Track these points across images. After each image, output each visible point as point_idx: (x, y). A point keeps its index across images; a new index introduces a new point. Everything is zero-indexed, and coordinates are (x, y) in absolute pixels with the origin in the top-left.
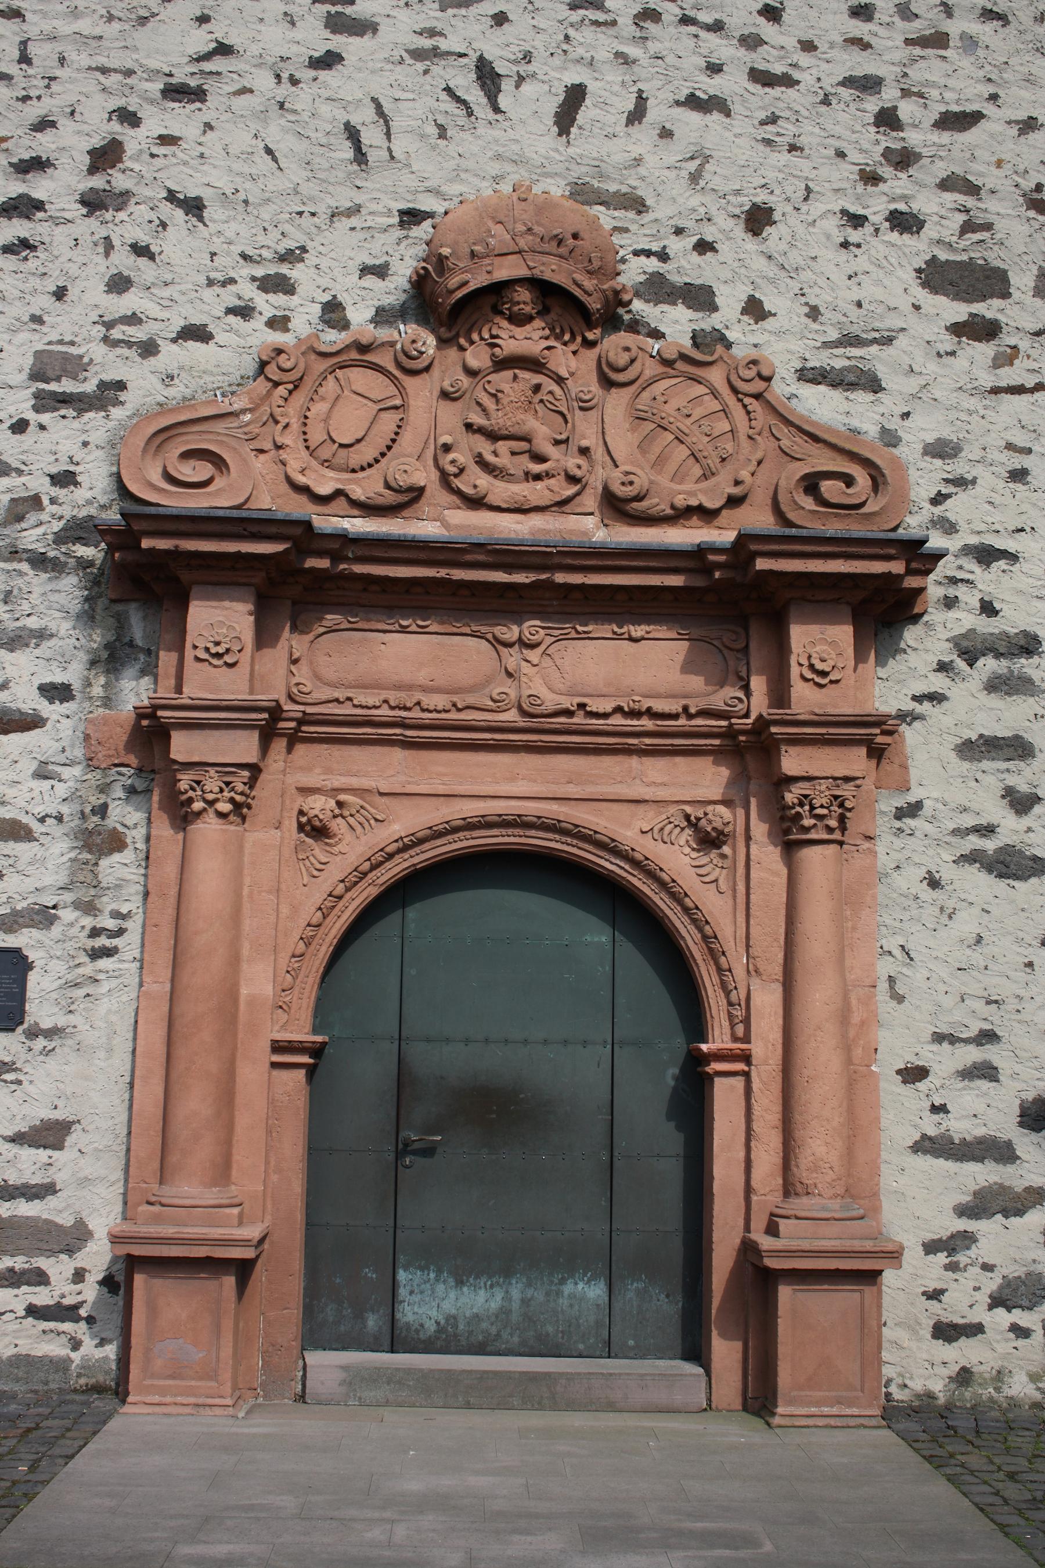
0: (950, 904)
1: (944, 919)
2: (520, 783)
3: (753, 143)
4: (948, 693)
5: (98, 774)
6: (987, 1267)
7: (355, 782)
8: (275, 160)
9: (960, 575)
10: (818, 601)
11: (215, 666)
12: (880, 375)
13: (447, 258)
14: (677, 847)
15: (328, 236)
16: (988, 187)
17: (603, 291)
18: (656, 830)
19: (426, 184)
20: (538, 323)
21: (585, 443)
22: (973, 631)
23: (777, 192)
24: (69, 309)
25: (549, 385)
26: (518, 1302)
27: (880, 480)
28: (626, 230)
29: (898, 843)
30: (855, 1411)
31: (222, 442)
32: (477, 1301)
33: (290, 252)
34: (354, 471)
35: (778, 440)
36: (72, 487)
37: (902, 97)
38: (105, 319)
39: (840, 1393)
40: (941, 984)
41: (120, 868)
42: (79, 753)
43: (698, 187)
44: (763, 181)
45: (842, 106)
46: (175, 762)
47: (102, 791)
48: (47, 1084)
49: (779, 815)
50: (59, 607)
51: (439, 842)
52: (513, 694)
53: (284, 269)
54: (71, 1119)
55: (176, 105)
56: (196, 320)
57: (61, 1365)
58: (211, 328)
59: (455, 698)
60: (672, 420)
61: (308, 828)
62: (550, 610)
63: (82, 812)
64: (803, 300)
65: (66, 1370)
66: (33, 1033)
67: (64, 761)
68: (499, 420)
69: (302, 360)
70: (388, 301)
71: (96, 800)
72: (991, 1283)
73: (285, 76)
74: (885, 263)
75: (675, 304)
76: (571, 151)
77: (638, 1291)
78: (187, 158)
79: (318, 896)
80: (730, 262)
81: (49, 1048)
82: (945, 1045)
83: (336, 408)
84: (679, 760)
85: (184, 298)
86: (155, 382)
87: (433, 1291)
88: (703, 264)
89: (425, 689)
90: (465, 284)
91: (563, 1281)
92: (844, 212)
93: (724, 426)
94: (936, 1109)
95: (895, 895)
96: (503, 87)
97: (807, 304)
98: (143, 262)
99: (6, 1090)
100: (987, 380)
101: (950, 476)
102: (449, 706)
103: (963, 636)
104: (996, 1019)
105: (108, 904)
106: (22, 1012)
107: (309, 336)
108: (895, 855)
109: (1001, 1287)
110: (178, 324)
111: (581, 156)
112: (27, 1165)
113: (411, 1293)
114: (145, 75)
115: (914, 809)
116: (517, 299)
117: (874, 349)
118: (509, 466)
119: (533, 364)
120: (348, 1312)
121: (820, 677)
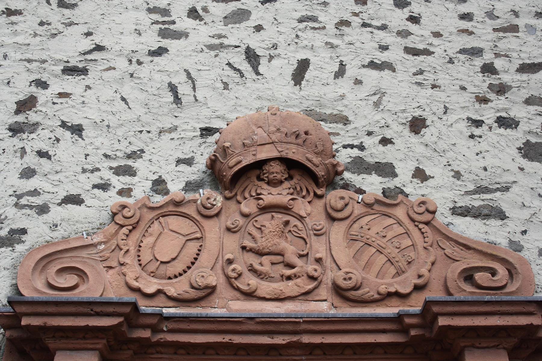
8: (127, 103)
12: (504, 209)
13: (228, 147)
19: (217, 114)
20: (286, 184)
21: (318, 255)
25: (294, 221)
27: (513, 272)
28: (338, 134)
33: (135, 152)
34: (170, 278)
35: (444, 249)
43: (379, 109)
44: (418, 105)
53: (130, 162)
58: (83, 197)
60: (374, 239)
64: (450, 168)
68: (262, 243)
70: (193, 178)
76: (302, 93)
78: (74, 104)
80: (403, 149)
83: (159, 240)
85: (68, 180)
88: (386, 151)
90: (240, 162)
92: (469, 119)
93: (407, 242)
98: (44, 160)
107: (143, 198)
110: (62, 194)
117: (498, 194)
119: (284, 209)
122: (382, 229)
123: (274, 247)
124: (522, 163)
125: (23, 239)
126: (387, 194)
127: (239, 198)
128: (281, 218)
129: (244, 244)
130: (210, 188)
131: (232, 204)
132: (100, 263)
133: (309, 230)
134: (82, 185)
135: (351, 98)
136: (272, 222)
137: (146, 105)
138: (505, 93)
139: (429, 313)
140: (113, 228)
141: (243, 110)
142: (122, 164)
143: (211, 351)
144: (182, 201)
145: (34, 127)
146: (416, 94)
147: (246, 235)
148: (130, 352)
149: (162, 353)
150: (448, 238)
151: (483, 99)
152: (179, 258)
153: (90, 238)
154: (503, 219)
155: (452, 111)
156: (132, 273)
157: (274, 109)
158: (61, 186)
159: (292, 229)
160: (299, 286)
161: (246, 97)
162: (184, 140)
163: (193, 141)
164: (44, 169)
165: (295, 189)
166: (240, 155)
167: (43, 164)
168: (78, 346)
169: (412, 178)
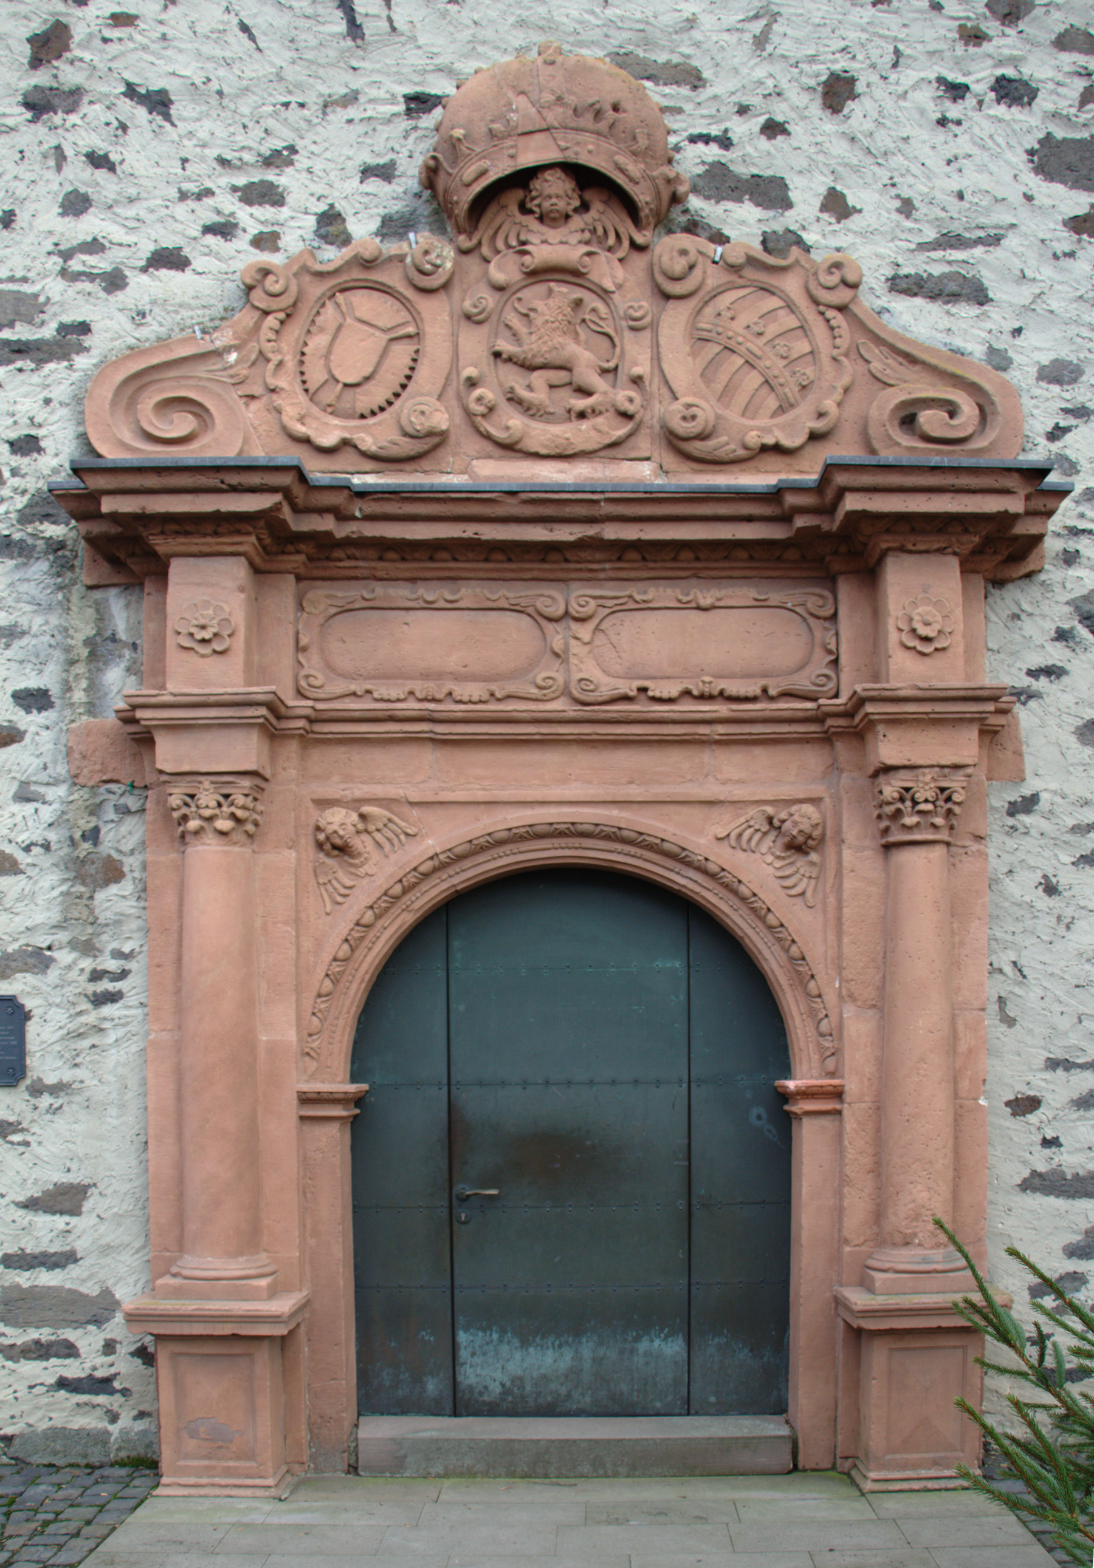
0: (1069, 912)
1: (1061, 930)
4: (1068, 667)
7: (379, 791)
8: (252, 38)
9: (1082, 525)
11: (203, 656)
12: (986, 283)
13: (459, 140)
14: (758, 855)
17: (653, 179)
18: (733, 836)
19: (438, 61)
20: (577, 222)
21: (637, 370)
23: (859, 57)
24: (18, 238)
25: (592, 301)
27: (988, 410)
28: (679, 111)
29: (1011, 843)
31: (204, 388)
32: (544, 1361)
33: (277, 153)
34: (363, 417)
35: (868, 362)
36: (35, 455)
38: (62, 248)
39: (937, 1455)
40: (1056, 1004)
41: (116, 900)
42: (62, 769)
43: (765, 54)
44: (842, 44)
46: (161, 772)
48: (57, 1145)
49: (876, 813)
50: (29, 599)
52: (560, 679)
53: (270, 176)
54: (86, 1182)
56: (169, 243)
57: (101, 1438)
58: (186, 252)
59: (493, 687)
60: (740, 339)
61: (328, 846)
62: (602, 575)
63: (72, 839)
64: (893, 192)
65: (105, 1443)
66: (37, 1090)
67: (46, 779)
68: (533, 346)
70: (396, 208)
71: (86, 823)
74: (990, 143)
75: (740, 200)
76: (610, 12)
78: (145, 41)
79: (343, 926)
80: (805, 147)
81: (56, 1105)
82: (1060, 1072)
83: (338, 341)
85: (153, 217)
86: (123, 322)
88: (773, 151)
89: (458, 678)
90: (483, 173)
91: (637, 1339)
92: (941, 80)
93: (802, 346)
94: (1047, 1143)
95: (1007, 904)
98: (101, 174)
99: (13, 1153)
101: (1069, 406)
102: (485, 696)
103: (1085, 598)
105: (108, 942)
107: (301, 253)
108: (1006, 858)
110: (147, 249)
111: (622, 19)
112: (46, 1231)
113: (473, 1354)
115: (1029, 803)
116: (548, 191)
117: (978, 251)
118: (547, 402)
119: (571, 274)
120: (405, 1376)
121: (924, 644)
122: (756, 320)
123: (554, 353)
124: (1031, 185)
125: (86, 345)
126: (770, 245)
127: (485, 250)
128: (565, 293)
129: (497, 348)
130: (431, 231)
131: (472, 263)
132: (232, 389)
133: (621, 319)
134: (182, 226)
135: (708, 27)
136: (550, 303)
137: (292, 41)
138: (1018, 19)
139: (828, 488)
140: (246, 318)
141: (491, 53)
142: (256, 180)
143: (444, 555)
144: (376, 259)
145: (72, 98)
146: (840, 17)
147: (502, 328)
148: (301, 558)
149: (356, 559)
150: (878, 340)
151: (973, 33)
152: (377, 377)
153: (207, 337)
154: (981, 304)
155: (910, 62)
156: (293, 407)
157: (551, 51)
158: (143, 229)
159: (587, 317)
160: (599, 431)
161: (494, 22)
162: (374, 124)
163: (391, 126)
164: (104, 193)
165: (594, 231)
166: (484, 157)
167: (102, 182)
168: (206, 549)
169: (821, 211)
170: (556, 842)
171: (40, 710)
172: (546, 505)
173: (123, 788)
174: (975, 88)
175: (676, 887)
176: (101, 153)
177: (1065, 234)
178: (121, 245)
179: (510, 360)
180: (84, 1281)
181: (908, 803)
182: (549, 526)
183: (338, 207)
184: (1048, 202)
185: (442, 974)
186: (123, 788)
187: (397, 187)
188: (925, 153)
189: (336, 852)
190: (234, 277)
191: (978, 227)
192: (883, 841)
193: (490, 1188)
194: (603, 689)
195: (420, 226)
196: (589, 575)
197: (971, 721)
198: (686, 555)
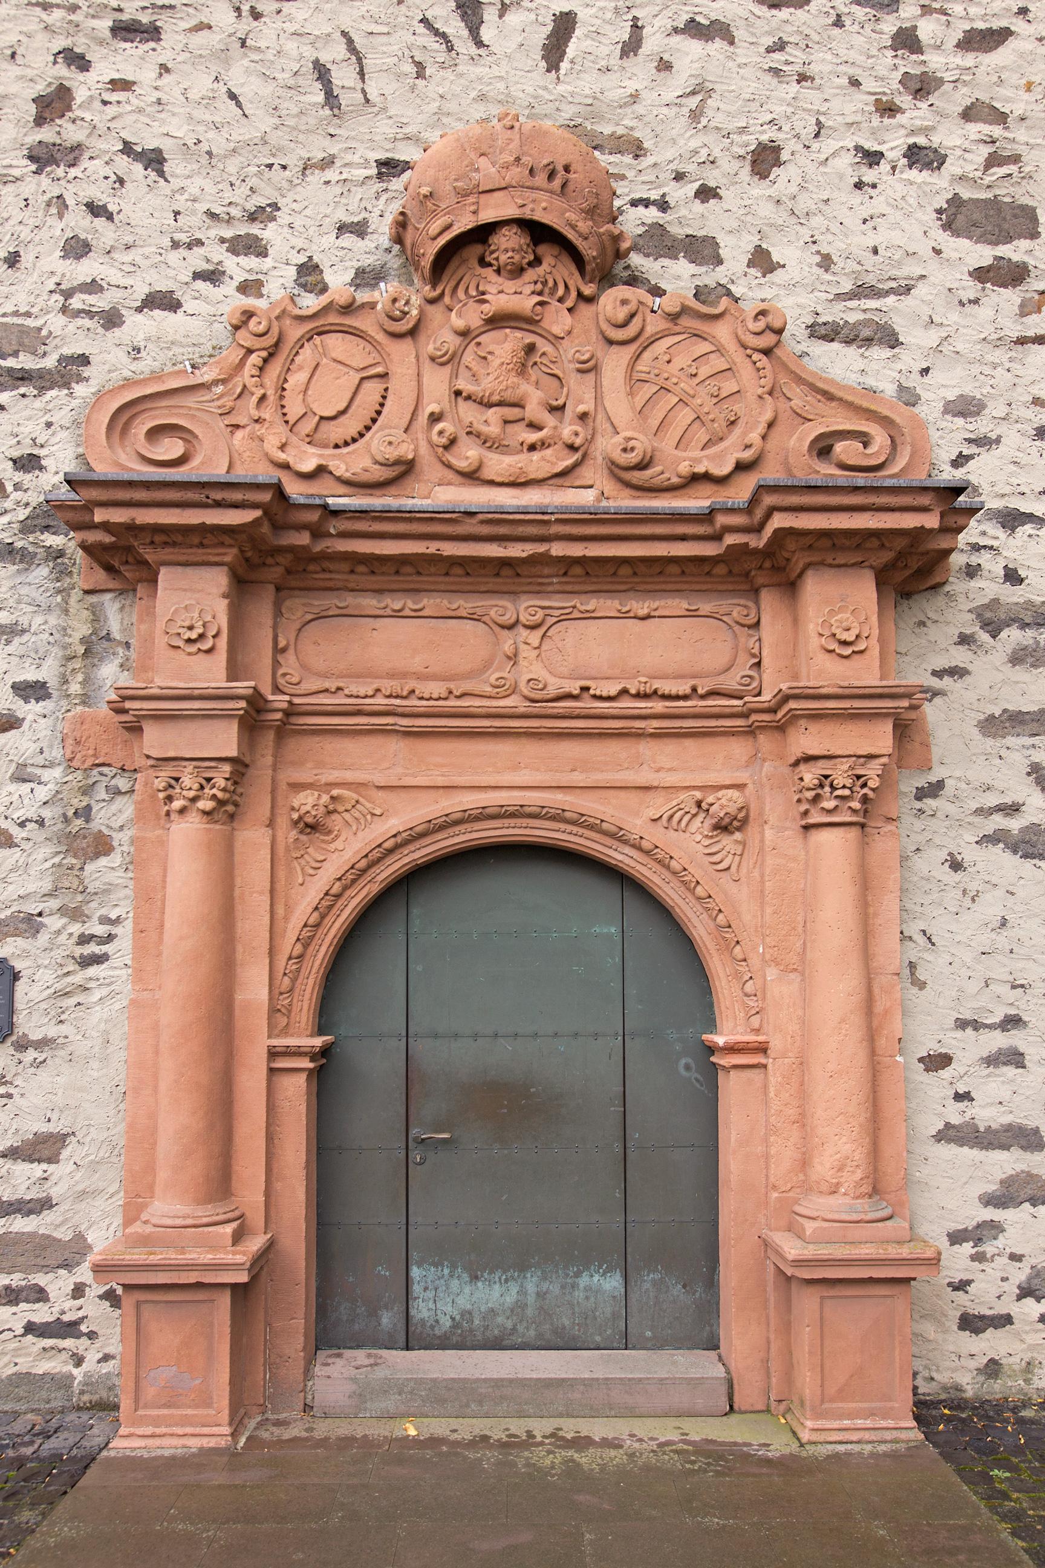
0: (973, 887)
1: (967, 902)
2: (524, 771)
3: (759, 74)
4: (970, 667)
5: (79, 775)
6: (1015, 1258)
7: (349, 776)
8: (239, 105)
9: (983, 542)
10: (839, 566)
11: (190, 654)
12: (897, 329)
15: (301, 192)
16: (1016, 113)
17: (599, 235)
18: (665, 817)
19: (407, 130)
20: (531, 274)
22: (996, 601)
25: (543, 346)
26: (534, 1295)
27: (898, 441)
28: (623, 177)
29: (918, 825)
30: (890, 1423)
32: (493, 1296)
34: (337, 446)
35: (790, 399)
36: (37, 472)
37: (922, 15)
38: (63, 287)
39: (874, 1405)
41: (103, 871)
42: (57, 753)
43: (700, 126)
44: (769, 117)
45: (856, 27)
47: (84, 793)
48: (39, 1098)
49: (796, 798)
51: (439, 836)
53: (255, 229)
55: (128, 45)
56: (163, 286)
57: (63, 1382)
58: (178, 295)
62: (550, 588)
63: (65, 815)
64: (815, 248)
69: (275, 323)
70: (369, 262)
71: (79, 802)
72: (1020, 1274)
73: (245, 8)
76: (561, 88)
77: (654, 1283)
78: (142, 104)
80: (734, 210)
81: (41, 1059)
82: (969, 1031)
84: (688, 743)
85: (148, 263)
86: (120, 357)
87: (447, 1287)
88: (706, 214)
91: (578, 1275)
92: (858, 148)
94: (959, 1097)
95: (916, 879)
96: (485, 17)
97: (818, 252)
98: (100, 222)
100: (1014, 331)
101: (972, 436)
102: (444, 695)
103: (986, 607)
104: (1022, 1004)
105: (95, 910)
106: (11, 1025)
109: (1030, 1279)
110: (141, 292)
112: (21, 1181)
113: (426, 1289)
114: (91, 11)
117: (891, 299)
122: (690, 362)
124: (939, 240)
125: (85, 375)
127: (447, 299)
133: (570, 362)
134: (174, 272)
136: (505, 345)
138: (928, 93)
141: (454, 124)
142: (242, 233)
145: (73, 154)
146: (768, 93)
150: (800, 380)
152: (351, 411)
153: (196, 371)
158: (138, 274)
159: (538, 360)
163: (365, 187)
164: (103, 240)
165: (545, 283)
170: (506, 822)
171: (37, 700)
172: (501, 525)
173: (115, 771)
174: (889, 155)
175: (614, 862)
176: (100, 203)
177: (971, 283)
178: (118, 287)
179: (468, 398)
180: (58, 1226)
181: (827, 789)
182: (504, 544)
183: (316, 259)
184: (955, 255)
185: (402, 937)
186: (115, 771)
187: (368, 243)
188: (843, 214)
189: (309, 830)
190: (222, 319)
191: (890, 279)
192: (803, 823)
193: (443, 1132)
194: (550, 688)
195: (390, 278)
196: (538, 588)
197: (887, 715)
198: (625, 570)
